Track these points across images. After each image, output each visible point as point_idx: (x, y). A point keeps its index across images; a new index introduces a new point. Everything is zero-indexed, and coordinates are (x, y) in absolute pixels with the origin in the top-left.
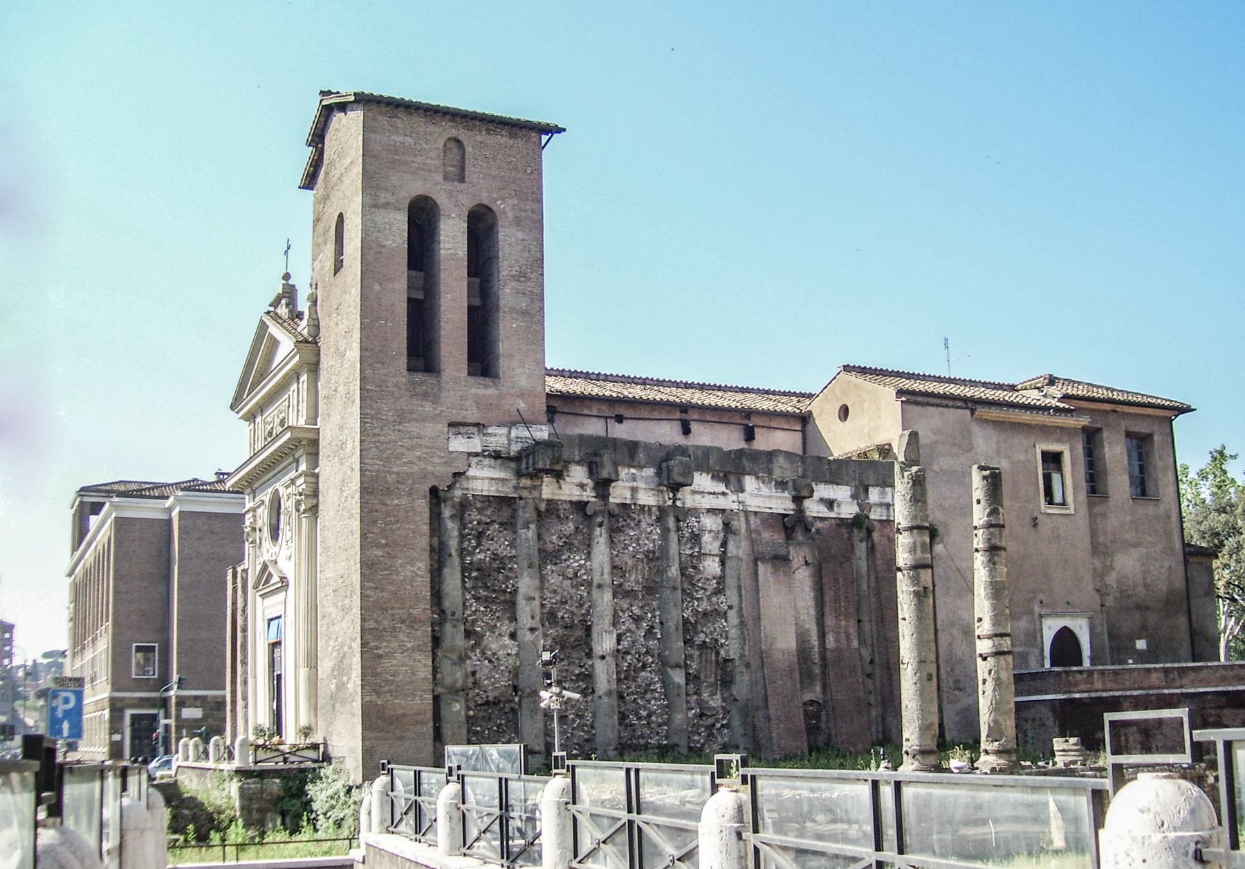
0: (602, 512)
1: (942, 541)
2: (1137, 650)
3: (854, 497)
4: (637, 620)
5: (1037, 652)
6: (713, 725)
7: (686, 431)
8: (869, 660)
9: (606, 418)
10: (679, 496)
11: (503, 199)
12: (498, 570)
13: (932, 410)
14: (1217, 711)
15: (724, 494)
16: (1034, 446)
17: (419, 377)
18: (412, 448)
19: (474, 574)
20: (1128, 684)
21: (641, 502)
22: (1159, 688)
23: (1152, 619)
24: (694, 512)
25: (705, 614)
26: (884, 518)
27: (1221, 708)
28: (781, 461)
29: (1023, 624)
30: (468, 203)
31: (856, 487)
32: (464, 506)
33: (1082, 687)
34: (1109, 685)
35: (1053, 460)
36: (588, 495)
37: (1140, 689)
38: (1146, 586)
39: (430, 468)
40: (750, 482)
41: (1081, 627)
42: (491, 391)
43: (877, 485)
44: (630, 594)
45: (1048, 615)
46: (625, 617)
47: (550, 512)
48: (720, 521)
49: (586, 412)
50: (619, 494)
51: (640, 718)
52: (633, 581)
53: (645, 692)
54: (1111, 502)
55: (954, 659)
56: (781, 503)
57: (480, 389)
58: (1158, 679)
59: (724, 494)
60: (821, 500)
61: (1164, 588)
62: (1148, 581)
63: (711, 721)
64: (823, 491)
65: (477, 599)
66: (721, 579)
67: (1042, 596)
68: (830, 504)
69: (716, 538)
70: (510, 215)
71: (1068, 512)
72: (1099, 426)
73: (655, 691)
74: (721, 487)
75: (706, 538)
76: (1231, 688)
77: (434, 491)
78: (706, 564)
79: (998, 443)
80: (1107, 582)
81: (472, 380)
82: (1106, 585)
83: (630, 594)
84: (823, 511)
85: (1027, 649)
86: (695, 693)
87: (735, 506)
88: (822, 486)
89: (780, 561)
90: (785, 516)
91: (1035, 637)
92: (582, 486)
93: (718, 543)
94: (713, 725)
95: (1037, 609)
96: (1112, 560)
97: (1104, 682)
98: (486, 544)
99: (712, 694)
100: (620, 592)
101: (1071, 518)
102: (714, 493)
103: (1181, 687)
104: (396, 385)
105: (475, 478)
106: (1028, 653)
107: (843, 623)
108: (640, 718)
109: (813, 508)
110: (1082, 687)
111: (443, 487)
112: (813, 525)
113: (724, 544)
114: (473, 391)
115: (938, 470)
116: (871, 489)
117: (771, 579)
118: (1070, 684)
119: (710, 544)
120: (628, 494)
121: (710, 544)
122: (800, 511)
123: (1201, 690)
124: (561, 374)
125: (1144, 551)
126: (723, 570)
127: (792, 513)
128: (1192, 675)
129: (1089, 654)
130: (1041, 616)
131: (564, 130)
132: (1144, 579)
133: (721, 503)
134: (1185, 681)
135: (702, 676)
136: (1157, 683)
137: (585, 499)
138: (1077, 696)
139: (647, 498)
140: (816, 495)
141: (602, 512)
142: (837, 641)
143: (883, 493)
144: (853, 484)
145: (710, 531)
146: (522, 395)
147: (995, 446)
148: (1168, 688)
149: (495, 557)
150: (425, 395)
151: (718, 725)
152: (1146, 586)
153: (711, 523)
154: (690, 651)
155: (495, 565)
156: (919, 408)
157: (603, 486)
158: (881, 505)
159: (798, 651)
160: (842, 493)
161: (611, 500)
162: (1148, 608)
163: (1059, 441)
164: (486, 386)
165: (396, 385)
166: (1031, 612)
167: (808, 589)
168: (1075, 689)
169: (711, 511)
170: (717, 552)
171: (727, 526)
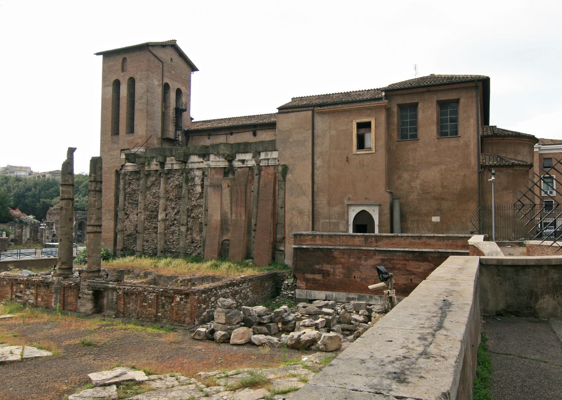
0: (163, 173)
1: (291, 173)
2: (433, 222)
3: (253, 157)
4: (173, 208)
5: (344, 222)
6: (197, 246)
7: (255, 135)
8: (254, 224)
9: (227, 134)
10: (187, 165)
11: (137, 74)
12: (134, 194)
13: (291, 114)
14: (404, 262)
15: (202, 162)
16: (352, 121)
17: (114, 137)
18: (112, 159)
19: (128, 195)
20: (338, 243)
21: (174, 168)
22: (360, 246)
23: (445, 205)
24: (192, 169)
25: (195, 206)
26: (266, 165)
27: (408, 260)
28: (222, 147)
29: (337, 209)
30: (127, 78)
31: (254, 153)
32: (125, 174)
33: (309, 243)
34: (326, 242)
35: (364, 126)
36: (158, 168)
37: (346, 246)
38: (443, 187)
39: (115, 164)
40: (212, 157)
41: (353, 211)
42: (132, 138)
43: (264, 151)
44: (171, 200)
45: (351, 205)
46: (169, 208)
47: (148, 175)
48: (201, 172)
49: (221, 133)
50: (167, 167)
51: (170, 242)
52: (172, 196)
53: (173, 234)
54: (420, 142)
55: (293, 225)
56: (223, 163)
57: (130, 138)
58: (359, 241)
59: (202, 162)
60: (239, 160)
61: (458, 187)
62: (445, 184)
63: (196, 245)
64: (240, 157)
65: (129, 203)
66: (202, 193)
67: (350, 196)
68: (243, 161)
69: (199, 179)
70: (138, 78)
71: (371, 152)
72: (416, 101)
73: (176, 233)
74: (201, 160)
75: (197, 179)
76: (421, 250)
77: (117, 171)
78: (197, 188)
79: (330, 123)
80: (413, 186)
81: (127, 135)
82: (412, 188)
83: (171, 200)
84: (240, 164)
85: (338, 221)
86: (191, 234)
87: (206, 166)
88: (240, 155)
89: (218, 187)
90: (225, 168)
91: (344, 215)
92: (157, 165)
93: (200, 180)
94: (197, 246)
95: (346, 202)
96: (417, 174)
97: (322, 241)
98: (131, 186)
99: (197, 235)
100: (168, 199)
101: (373, 154)
102: (198, 162)
103: (377, 246)
104: (108, 141)
105: (127, 166)
106: (339, 223)
107: (239, 210)
108: (170, 242)
109: (236, 164)
110: (309, 243)
111: (118, 170)
112: (236, 170)
113: (203, 180)
114: (127, 139)
115: (292, 141)
116: (261, 153)
117: (213, 193)
118: (302, 241)
119: (198, 181)
120: (170, 166)
121: (198, 181)
122: (231, 166)
123: (391, 249)
124: (309, 110)
125: (443, 167)
126: (202, 190)
127: (227, 166)
128: (386, 241)
129: (378, 224)
130: (348, 205)
131: (95, 54)
132: (442, 183)
133: (201, 166)
134: (379, 243)
135: (193, 228)
136: (358, 244)
137: (157, 169)
138: (304, 247)
139: (176, 167)
140: (237, 159)
141: (163, 173)
142: (236, 216)
143: (267, 155)
144: (252, 152)
145: (198, 176)
146: (140, 138)
147: (328, 125)
148: (365, 247)
149: (133, 190)
150: (115, 142)
151: (198, 246)
152: (443, 187)
153: (198, 173)
154: (189, 219)
155: (133, 192)
156: (285, 115)
157: (162, 164)
158: (265, 159)
159: (221, 220)
160: (248, 157)
161: (165, 169)
162: (443, 199)
163: (369, 116)
164: (130, 136)
165: (108, 141)
166: (343, 203)
167: (228, 196)
168: (304, 244)
169: (198, 169)
170: (200, 184)
171: (203, 173)
